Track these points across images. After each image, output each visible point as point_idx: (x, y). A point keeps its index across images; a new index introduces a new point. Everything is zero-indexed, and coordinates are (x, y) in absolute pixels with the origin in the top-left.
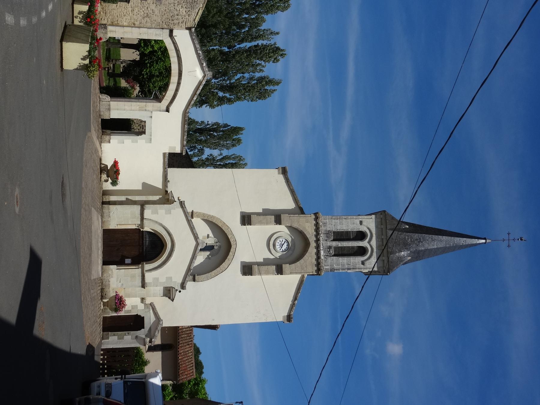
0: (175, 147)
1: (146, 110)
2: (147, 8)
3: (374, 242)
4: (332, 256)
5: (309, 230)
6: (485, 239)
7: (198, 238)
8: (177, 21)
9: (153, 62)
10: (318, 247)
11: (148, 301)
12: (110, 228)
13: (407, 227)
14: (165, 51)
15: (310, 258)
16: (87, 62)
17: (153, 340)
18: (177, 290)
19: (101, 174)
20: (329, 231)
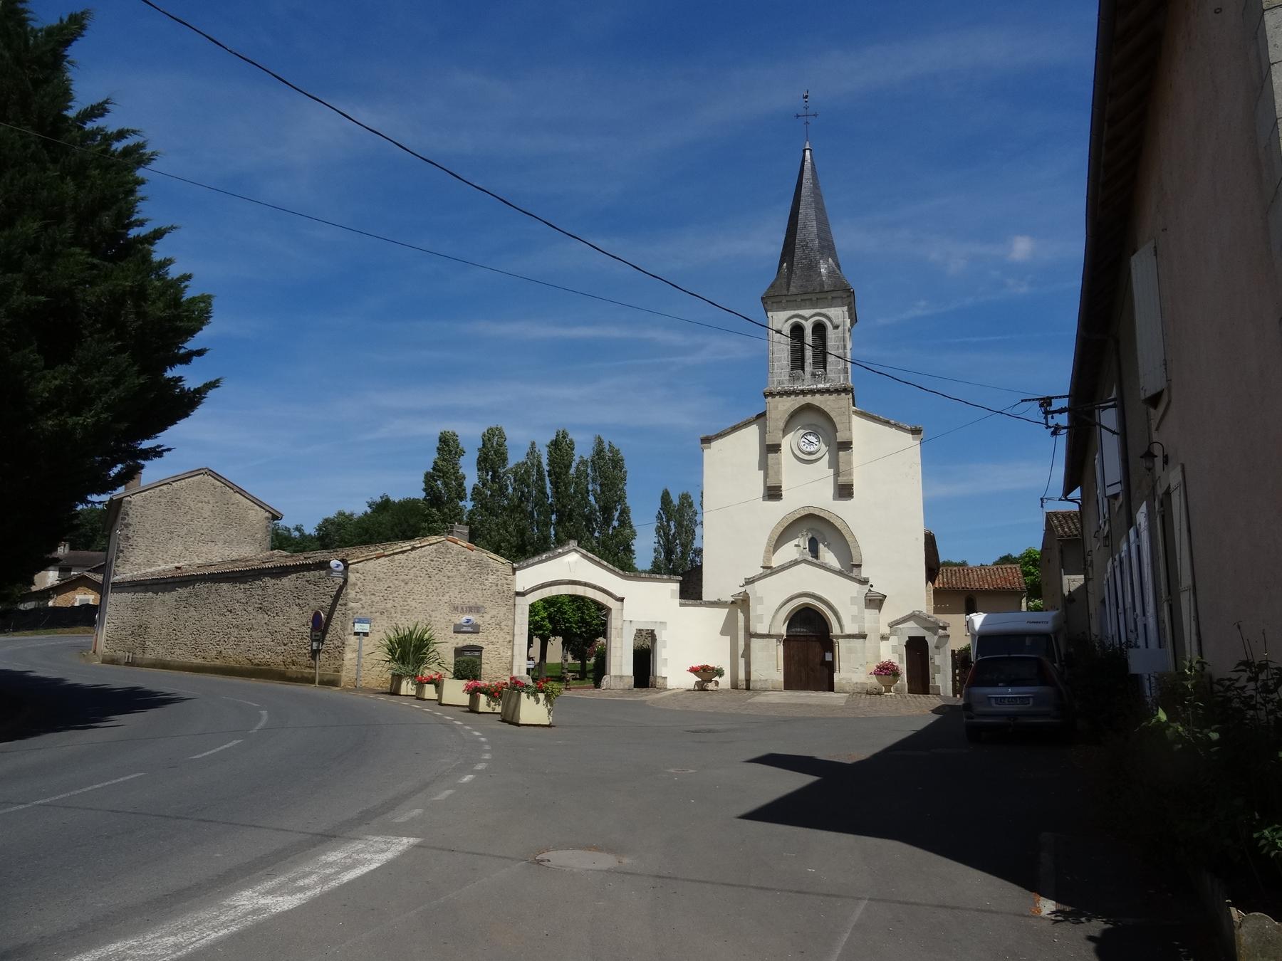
0: (672, 590)
1: (622, 629)
2: (489, 624)
3: (806, 312)
4: (826, 371)
5: (787, 405)
6: (804, 151)
7: (796, 560)
8: (505, 586)
9: (563, 618)
10: (813, 392)
11: (886, 630)
12: (783, 680)
13: (785, 265)
14: (549, 602)
15: (828, 403)
16: (541, 696)
17: (941, 625)
18: (870, 590)
19: (708, 690)
20: (790, 377)
